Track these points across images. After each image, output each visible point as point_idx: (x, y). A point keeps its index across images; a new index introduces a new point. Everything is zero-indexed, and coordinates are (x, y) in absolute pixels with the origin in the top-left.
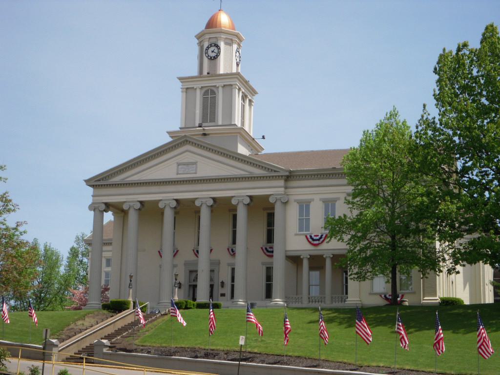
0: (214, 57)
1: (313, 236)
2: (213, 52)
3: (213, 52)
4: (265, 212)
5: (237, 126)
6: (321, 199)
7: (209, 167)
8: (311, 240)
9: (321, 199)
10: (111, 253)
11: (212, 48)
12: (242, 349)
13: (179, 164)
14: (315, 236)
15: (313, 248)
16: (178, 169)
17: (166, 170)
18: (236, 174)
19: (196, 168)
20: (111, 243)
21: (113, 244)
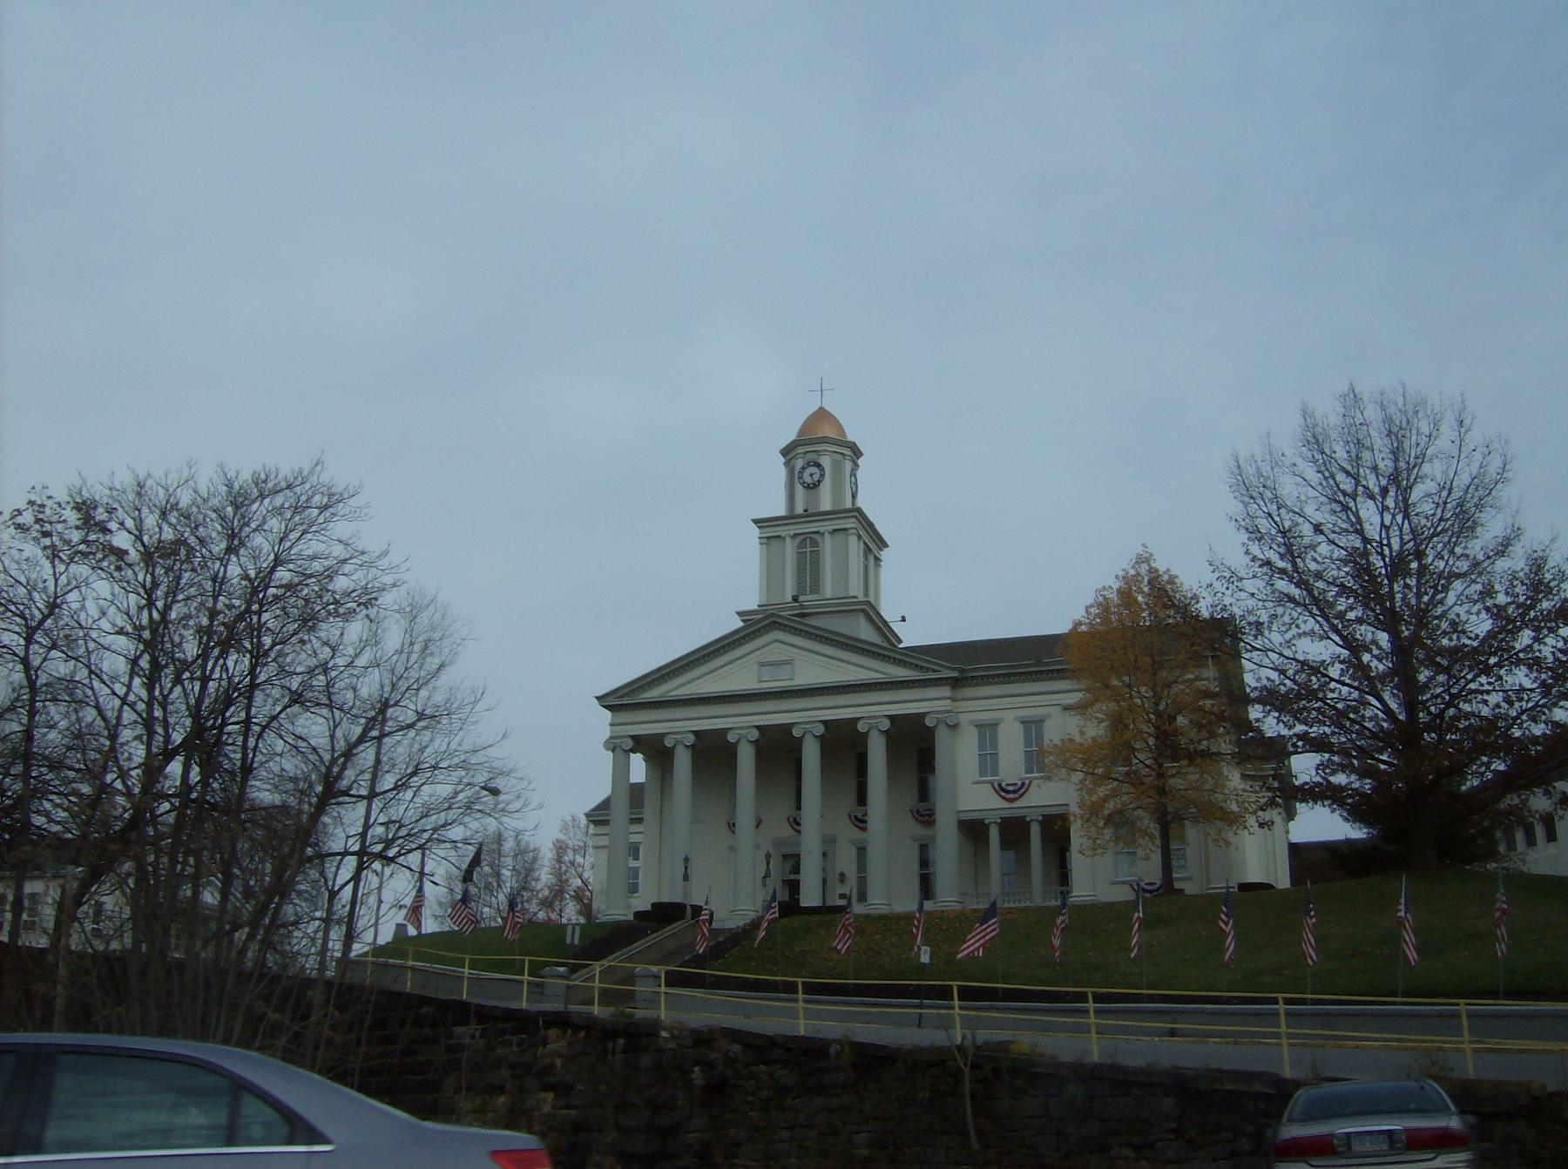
6: (1016, 719)
9: (1016, 719)
15: (1006, 805)
17: (739, 675)
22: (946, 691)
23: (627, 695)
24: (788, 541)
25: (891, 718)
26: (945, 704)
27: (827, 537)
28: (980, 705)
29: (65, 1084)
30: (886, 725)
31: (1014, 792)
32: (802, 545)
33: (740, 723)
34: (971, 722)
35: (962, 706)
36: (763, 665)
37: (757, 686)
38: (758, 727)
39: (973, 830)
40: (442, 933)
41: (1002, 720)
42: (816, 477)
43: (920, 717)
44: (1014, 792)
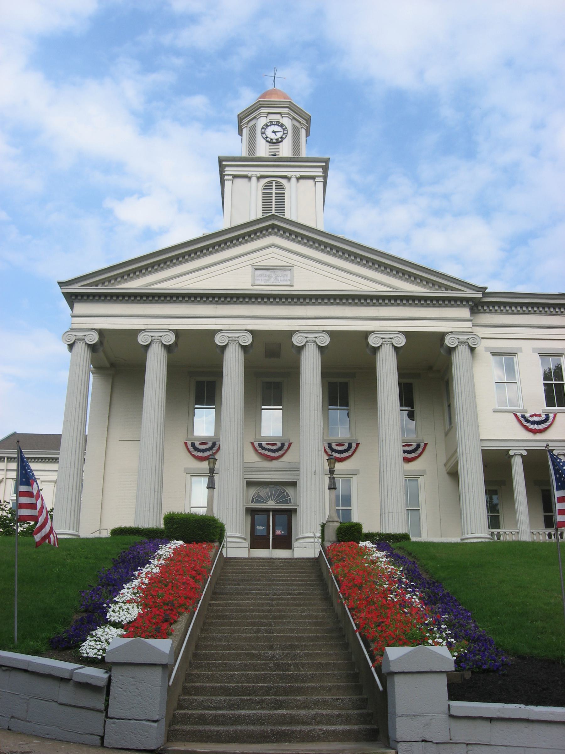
0: (282, 138)
1: (527, 416)
2: (274, 132)
3: (274, 132)
4: (428, 375)
5: (321, 552)
6: (534, 350)
7: (314, 273)
8: (525, 421)
9: (534, 350)
10: (56, 473)
11: (276, 126)
12: (403, 744)
13: (257, 268)
14: (531, 416)
15: (530, 436)
16: (253, 276)
17: (230, 272)
18: (366, 288)
19: (292, 276)
20: (57, 459)
21: (60, 461)
22: (465, 313)
23: (102, 282)
24: (254, 179)
25: (407, 334)
26: (466, 326)
27: (294, 180)
28: (495, 331)
29: (217, 457)
30: (401, 341)
31: (538, 423)
32: (268, 186)
33: (233, 326)
34: (487, 349)
35: (482, 332)
36: (256, 269)
37: (251, 288)
38: (251, 332)
39: (496, 465)
40: (533, 543)
41: (520, 350)
42: (279, 135)
43: (442, 336)
44: (538, 423)
